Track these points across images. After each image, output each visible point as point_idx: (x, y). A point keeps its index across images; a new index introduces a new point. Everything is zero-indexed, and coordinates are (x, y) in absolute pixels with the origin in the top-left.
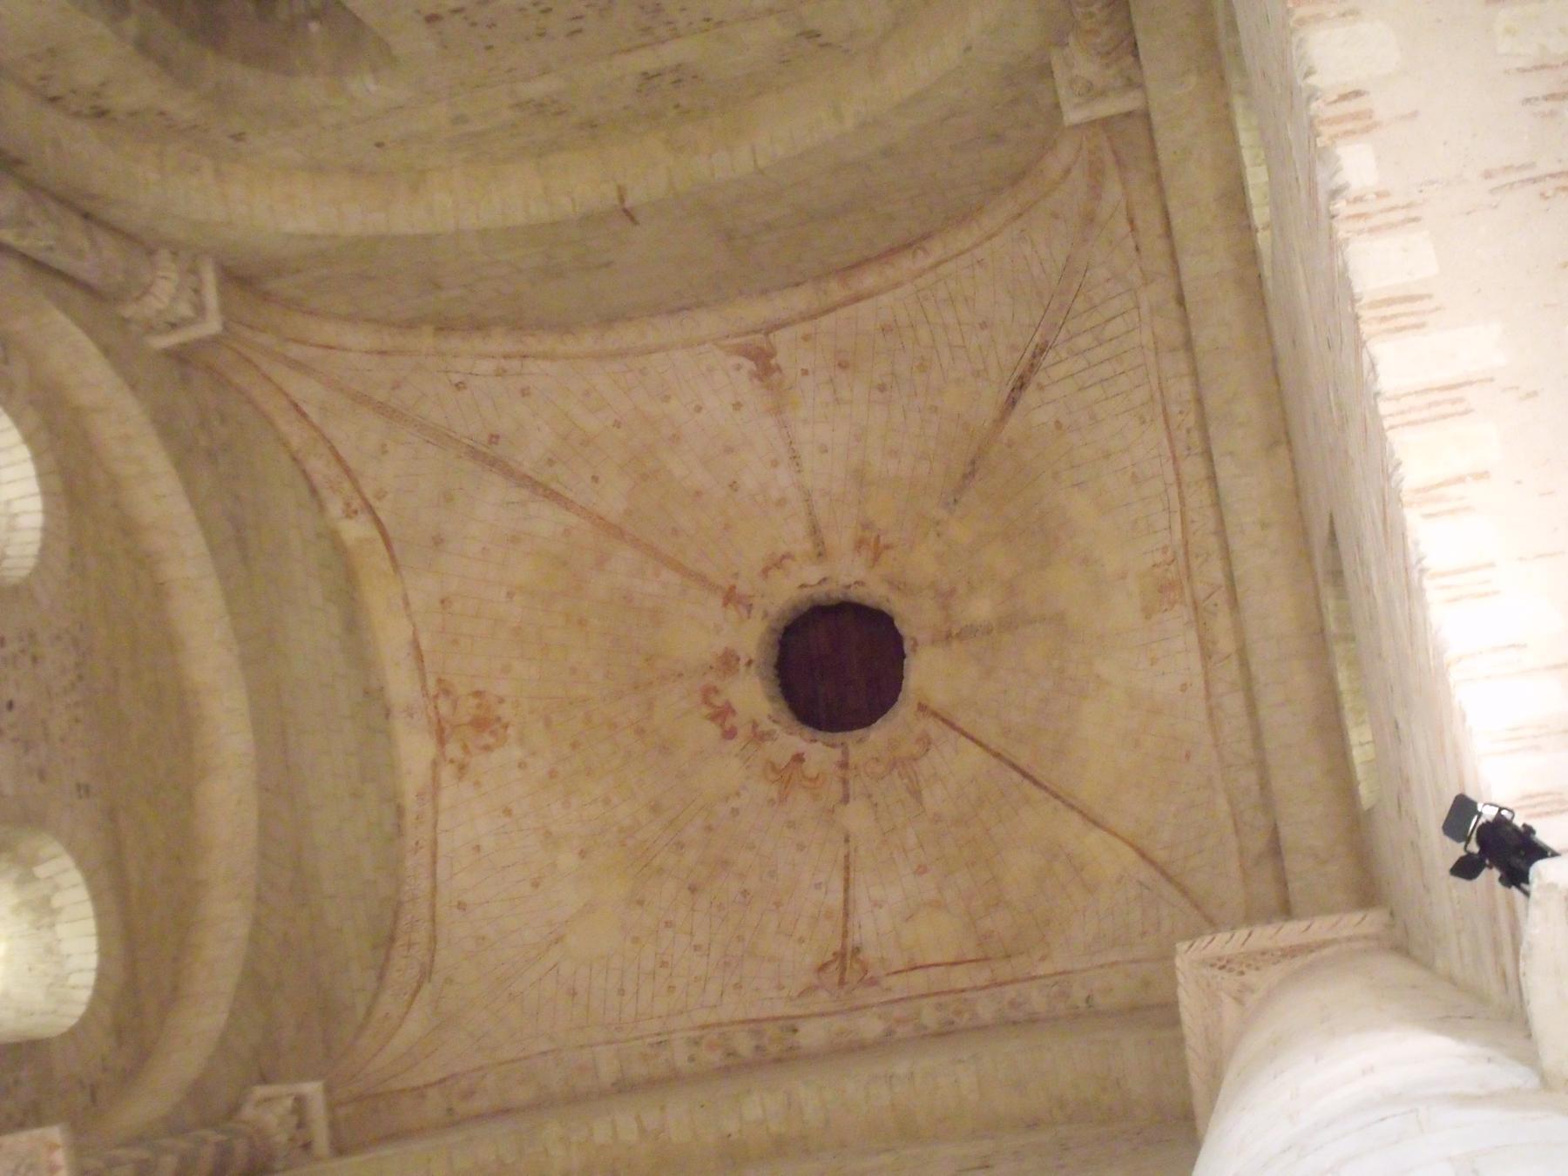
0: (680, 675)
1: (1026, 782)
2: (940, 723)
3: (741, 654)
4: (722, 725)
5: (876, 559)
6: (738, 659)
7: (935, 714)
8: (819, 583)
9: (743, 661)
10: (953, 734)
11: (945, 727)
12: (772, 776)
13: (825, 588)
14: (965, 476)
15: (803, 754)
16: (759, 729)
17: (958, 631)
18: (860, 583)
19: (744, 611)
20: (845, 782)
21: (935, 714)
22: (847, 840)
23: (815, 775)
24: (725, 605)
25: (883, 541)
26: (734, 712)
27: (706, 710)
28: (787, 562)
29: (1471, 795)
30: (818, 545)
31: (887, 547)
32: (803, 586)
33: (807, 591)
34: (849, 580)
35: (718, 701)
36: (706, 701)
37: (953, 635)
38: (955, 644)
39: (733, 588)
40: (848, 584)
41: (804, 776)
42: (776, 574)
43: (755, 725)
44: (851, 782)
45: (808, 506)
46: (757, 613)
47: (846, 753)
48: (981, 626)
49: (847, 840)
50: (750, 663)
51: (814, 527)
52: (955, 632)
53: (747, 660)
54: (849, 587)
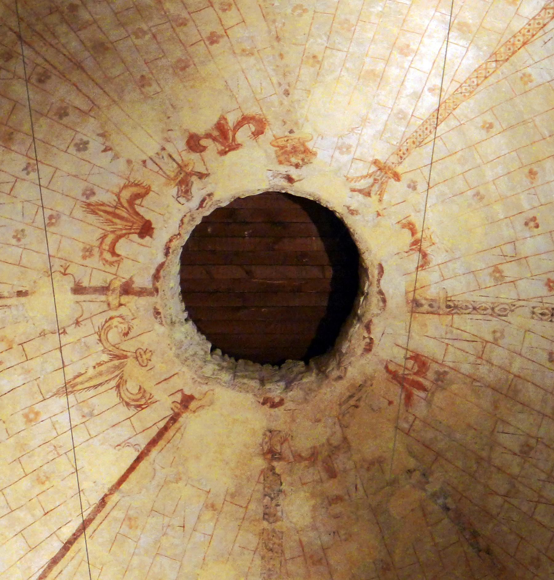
0: (287, 93)
1: (56, 546)
2: (162, 425)
3: (304, 171)
4: (208, 136)
5: (394, 376)
6: (297, 166)
7: (174, 419)
8: (381, 293)
9: (294, 173)
10: (143, 441)
11: (154, 432)
12: (126, 195)
13: (374, 299)
14: (475, 535)
15: (151, 237)
16: (194, 179)
17: (277, 471)
18: (368, 348)
19: (363, 184)
20: (104, 290)
21: (174, 419)
22: (20, 294)
23: (118, 251)
24: (375, 162)
25: (418, 394)
26: (223, 153)
27: (232, 119)
28: (416, 256)
29: (215, 194)
30: (431, 306)
31: (409, 397)
32: (381, 270)
33: (373, 272)
34: (376, 332)
35: (242, 136)
36: (245, 120)
37: (275, 464)
38: (260, 463)
39: (397, 177)
40: (372, 327)
41: (121, 237)
42: (407, 238)
43: (201, 176)
44: (103, 298)
45: (486, 309)
46: (356, 201)
47: (141, 292)
48: (278, 505)
49: (20, 294)
50: (290, 179)
51: (456, 307)
52: (279, 466)
53: (294, 177)
54: (368, 328)
